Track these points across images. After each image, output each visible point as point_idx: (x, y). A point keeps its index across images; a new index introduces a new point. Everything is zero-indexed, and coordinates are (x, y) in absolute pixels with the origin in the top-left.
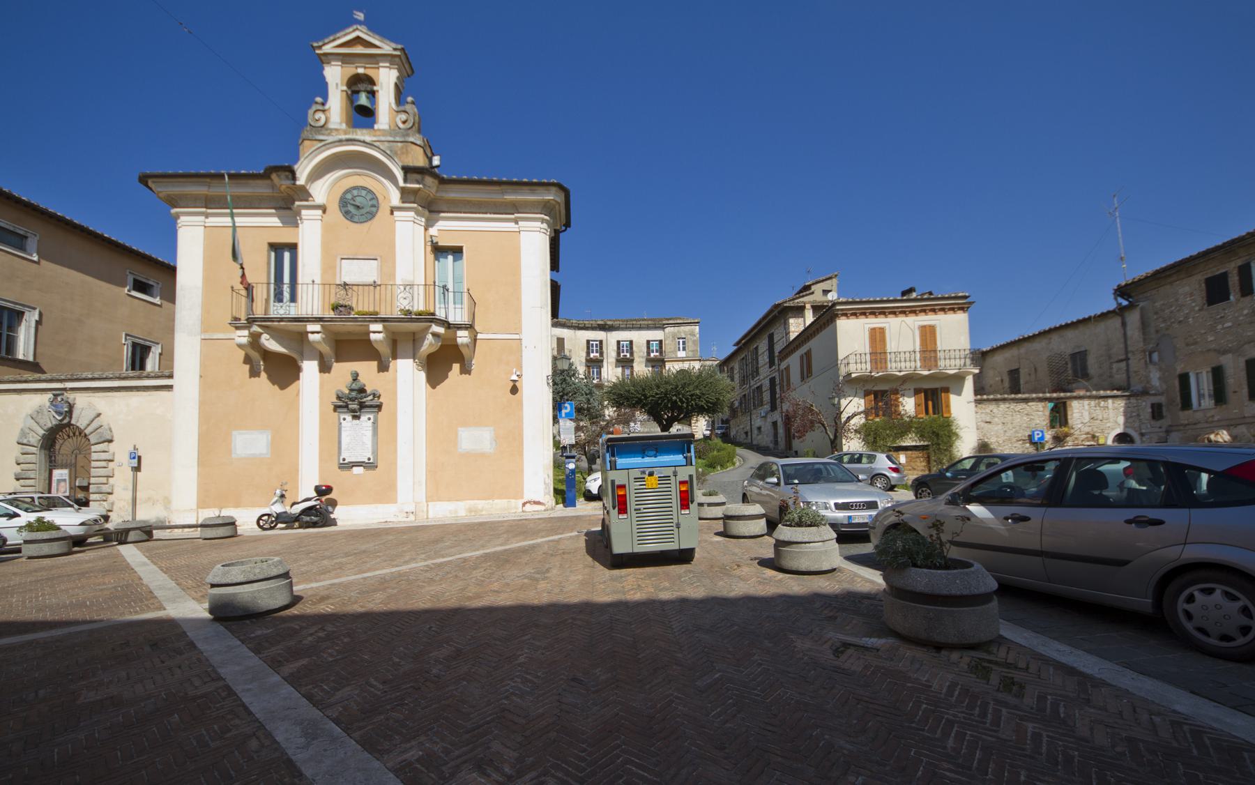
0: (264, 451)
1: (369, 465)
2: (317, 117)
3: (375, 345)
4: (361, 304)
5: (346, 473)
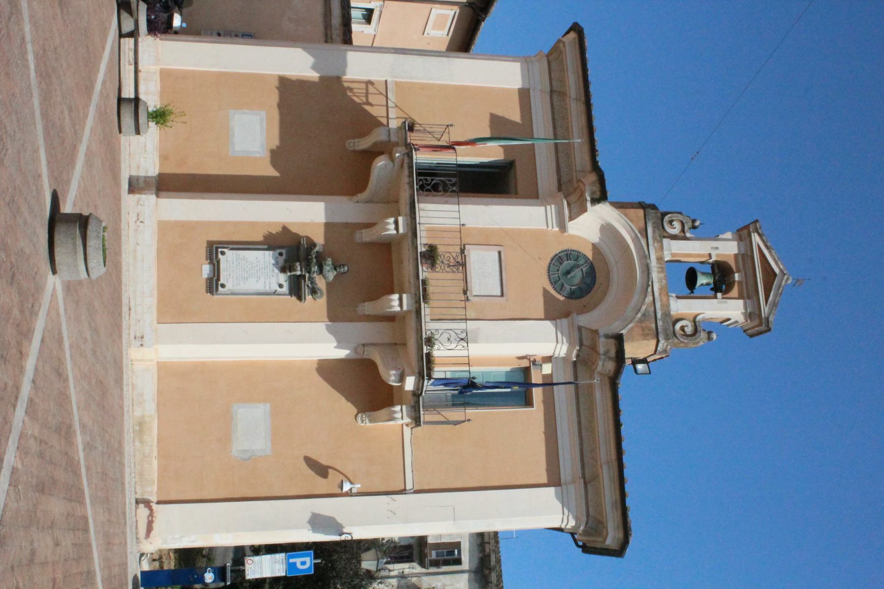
0: (237, 148)
1: (213, 284)
2: (677, 224)
3: (385, 298)
4: (438, 280)
5: (203, 252)
